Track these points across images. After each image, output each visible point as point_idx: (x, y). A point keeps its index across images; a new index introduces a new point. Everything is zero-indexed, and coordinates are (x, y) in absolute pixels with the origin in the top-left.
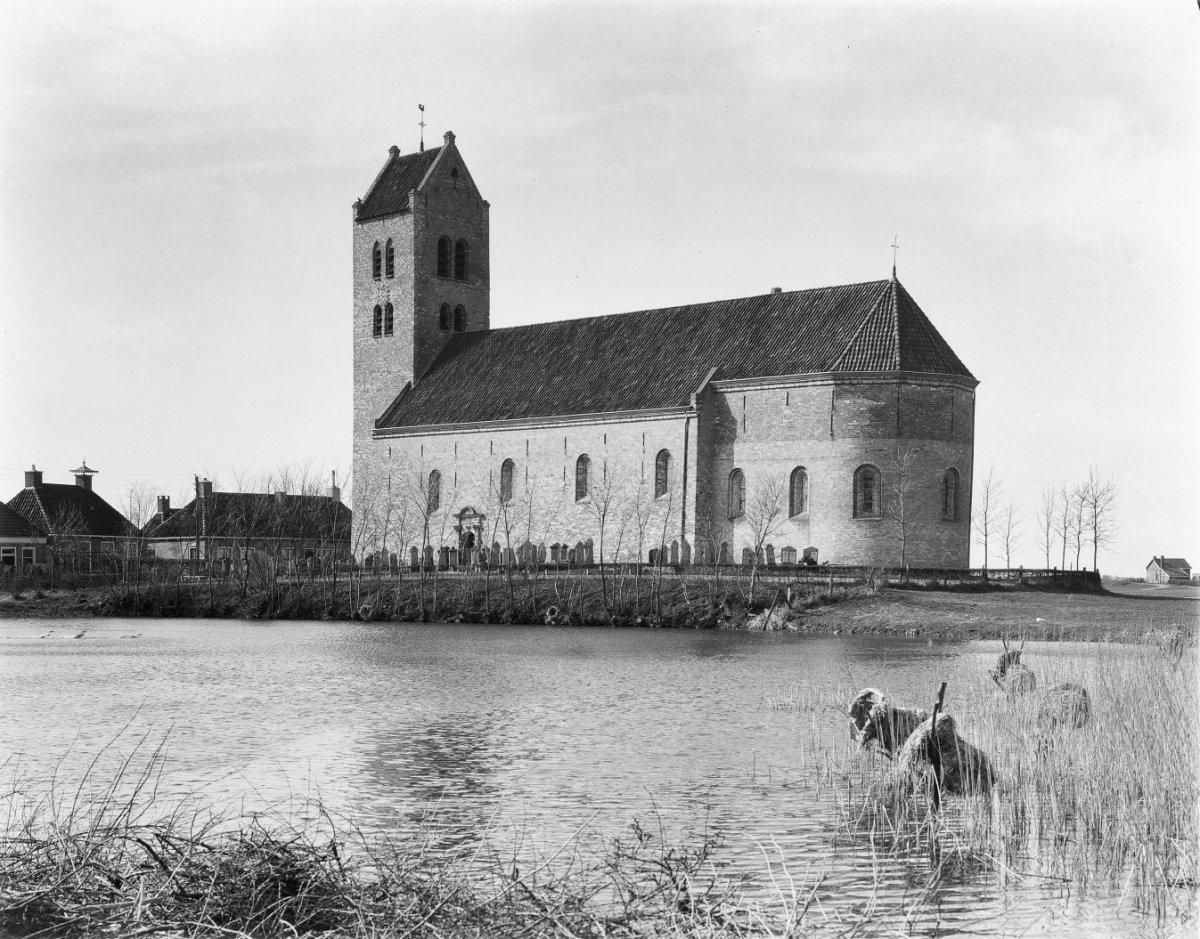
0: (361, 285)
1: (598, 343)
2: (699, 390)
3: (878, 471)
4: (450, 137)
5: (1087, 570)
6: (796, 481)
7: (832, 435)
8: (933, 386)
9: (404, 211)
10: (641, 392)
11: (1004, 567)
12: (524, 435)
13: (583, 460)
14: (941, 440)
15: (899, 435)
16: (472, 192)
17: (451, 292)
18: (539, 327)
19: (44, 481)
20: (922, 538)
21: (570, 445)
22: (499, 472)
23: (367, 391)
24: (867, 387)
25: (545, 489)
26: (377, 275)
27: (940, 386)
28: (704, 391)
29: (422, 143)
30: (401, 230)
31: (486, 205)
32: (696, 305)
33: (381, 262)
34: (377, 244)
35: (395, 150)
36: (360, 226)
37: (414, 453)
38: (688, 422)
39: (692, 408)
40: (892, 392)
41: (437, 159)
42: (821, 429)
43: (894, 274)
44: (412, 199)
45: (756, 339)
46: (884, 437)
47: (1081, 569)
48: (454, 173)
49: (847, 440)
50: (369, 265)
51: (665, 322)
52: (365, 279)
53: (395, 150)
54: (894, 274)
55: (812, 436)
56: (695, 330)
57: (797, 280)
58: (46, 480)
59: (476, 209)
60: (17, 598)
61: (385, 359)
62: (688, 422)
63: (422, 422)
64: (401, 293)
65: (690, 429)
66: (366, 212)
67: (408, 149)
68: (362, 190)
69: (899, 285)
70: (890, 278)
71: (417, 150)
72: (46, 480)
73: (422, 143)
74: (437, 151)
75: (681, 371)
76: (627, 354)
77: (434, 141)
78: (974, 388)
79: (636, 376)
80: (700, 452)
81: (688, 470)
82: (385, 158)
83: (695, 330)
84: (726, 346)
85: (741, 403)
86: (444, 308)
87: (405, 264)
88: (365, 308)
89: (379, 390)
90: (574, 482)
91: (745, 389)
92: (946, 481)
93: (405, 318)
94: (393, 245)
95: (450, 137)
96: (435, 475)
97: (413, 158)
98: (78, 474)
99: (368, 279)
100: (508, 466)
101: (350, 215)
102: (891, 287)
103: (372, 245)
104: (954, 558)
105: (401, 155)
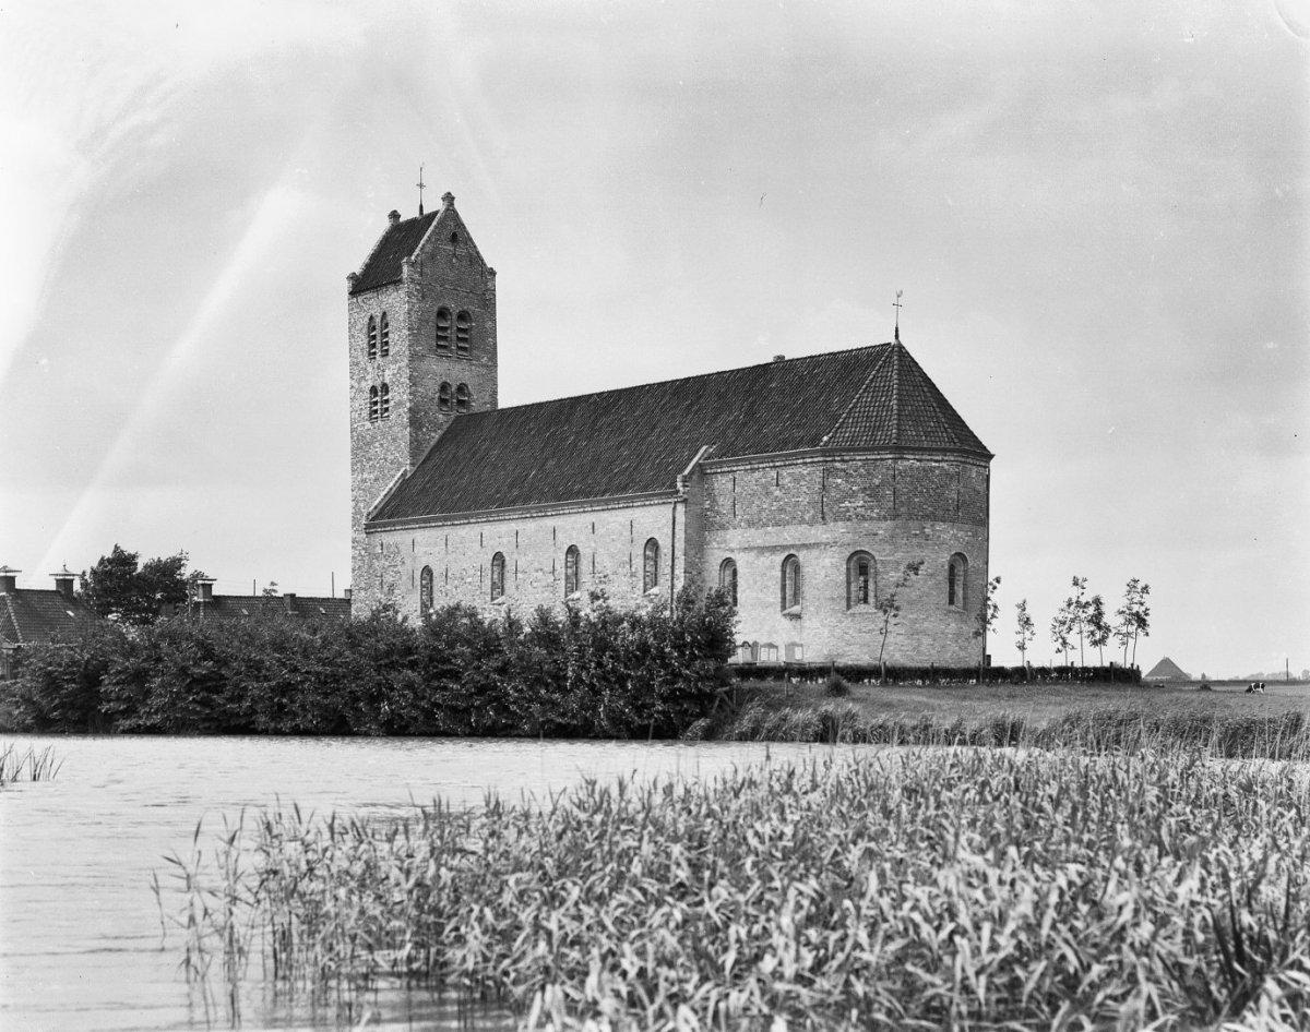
0: (357, 364)
1: (594, 423)
2: (686, 472)
3: (873, 557)
4: (449, 198)
5: (1075, 665)
6: (788, 571)
7: (823, 518)
8: (936, 461)
9: (397, 282)
10: (631, 474)
11: (251, 594)
12: (513, 526)
13: (572, 551)
14: (944, 521)
15: (895, 517)
16: (475, 259)
17: (457, 372)
18: (540, 405)
19: (17, 587)
20: (924, 632)
21: (559, 535)
22: (489, 566)
23: (364, 481)
24: (860, 463)
25: (535, 584)
26: (372, 355)
27: (943, 461)
28: (691, 473)
29: (421, 207)
30: (396, 303)
31: (493, 273)
32: (697, 377)
33: (376, 337)
34: (371, 318)
35: (394, 215)
36: (355, 300)
37: (405, 550)
38: (674, 509)
39: (678, 492)
40: (888, 469)
41: (434, 223)
42: (812, 512)
43: (897, 336)
44: (405, 269)
45: (751, 413)
46: (879, 519)
47: (1107, 664)
48: (454, 238)
49: (840, 523)
50: (363, 341)
51: (663, 396)
52: (360, 358)
53: (394, 215)
54: (897, 336)
55: (802, 521)
56: (692, 405)
57: (801, 344)
58: (19, 585)
59: (479, 278)
60: (1276, 951)
61: (381, 445)
62: (674, 509)
63: (413, 513)
64: (395, 371)
65: (677, 515)
66: (363, 284)
67: (409, 213)
68: (357, 267)
69: (901, 347)
70: (893, 341)
71: (416, 214)
72: (19, 585)
73: (421, 207)
74: (436, 213)
75: (672, 451)
76: (622, 433)
77: (435, 205)
78: (988, 462)
79: (628, 458)
80: (687, 541)
81: (676, 560)
82: (385, 225)
83: (692, 405)
84: (719, 422)
85: (730, 486)
86: (444, 387)
87: (399, 340)
88: (361, 390)
89: (376, 480)
90: (563, 577)
91: (735, 469)
92: (952, 568)
93: (400, 395)
94: (389, 318)
95: (449, 198)
96: (427, 571)
97: (413, 222)
98: (58, 577)
99: (363, 359)
100: (499, 559)
101: (346, 286)
102: (892, 351)
103: (367, 319)
104: (962, 654)
105: (401, 220)
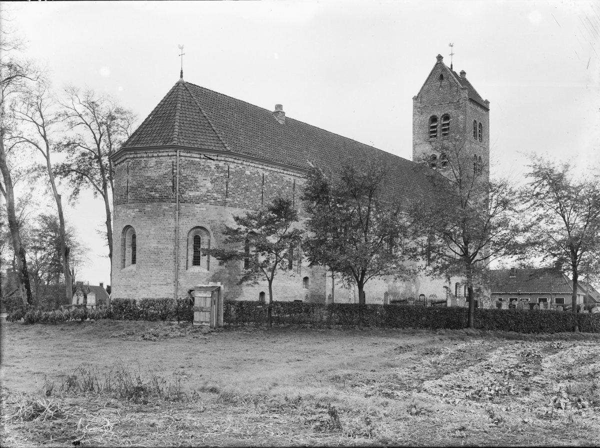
43: (182, 76)
